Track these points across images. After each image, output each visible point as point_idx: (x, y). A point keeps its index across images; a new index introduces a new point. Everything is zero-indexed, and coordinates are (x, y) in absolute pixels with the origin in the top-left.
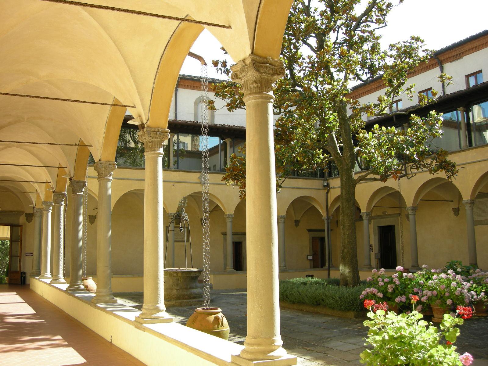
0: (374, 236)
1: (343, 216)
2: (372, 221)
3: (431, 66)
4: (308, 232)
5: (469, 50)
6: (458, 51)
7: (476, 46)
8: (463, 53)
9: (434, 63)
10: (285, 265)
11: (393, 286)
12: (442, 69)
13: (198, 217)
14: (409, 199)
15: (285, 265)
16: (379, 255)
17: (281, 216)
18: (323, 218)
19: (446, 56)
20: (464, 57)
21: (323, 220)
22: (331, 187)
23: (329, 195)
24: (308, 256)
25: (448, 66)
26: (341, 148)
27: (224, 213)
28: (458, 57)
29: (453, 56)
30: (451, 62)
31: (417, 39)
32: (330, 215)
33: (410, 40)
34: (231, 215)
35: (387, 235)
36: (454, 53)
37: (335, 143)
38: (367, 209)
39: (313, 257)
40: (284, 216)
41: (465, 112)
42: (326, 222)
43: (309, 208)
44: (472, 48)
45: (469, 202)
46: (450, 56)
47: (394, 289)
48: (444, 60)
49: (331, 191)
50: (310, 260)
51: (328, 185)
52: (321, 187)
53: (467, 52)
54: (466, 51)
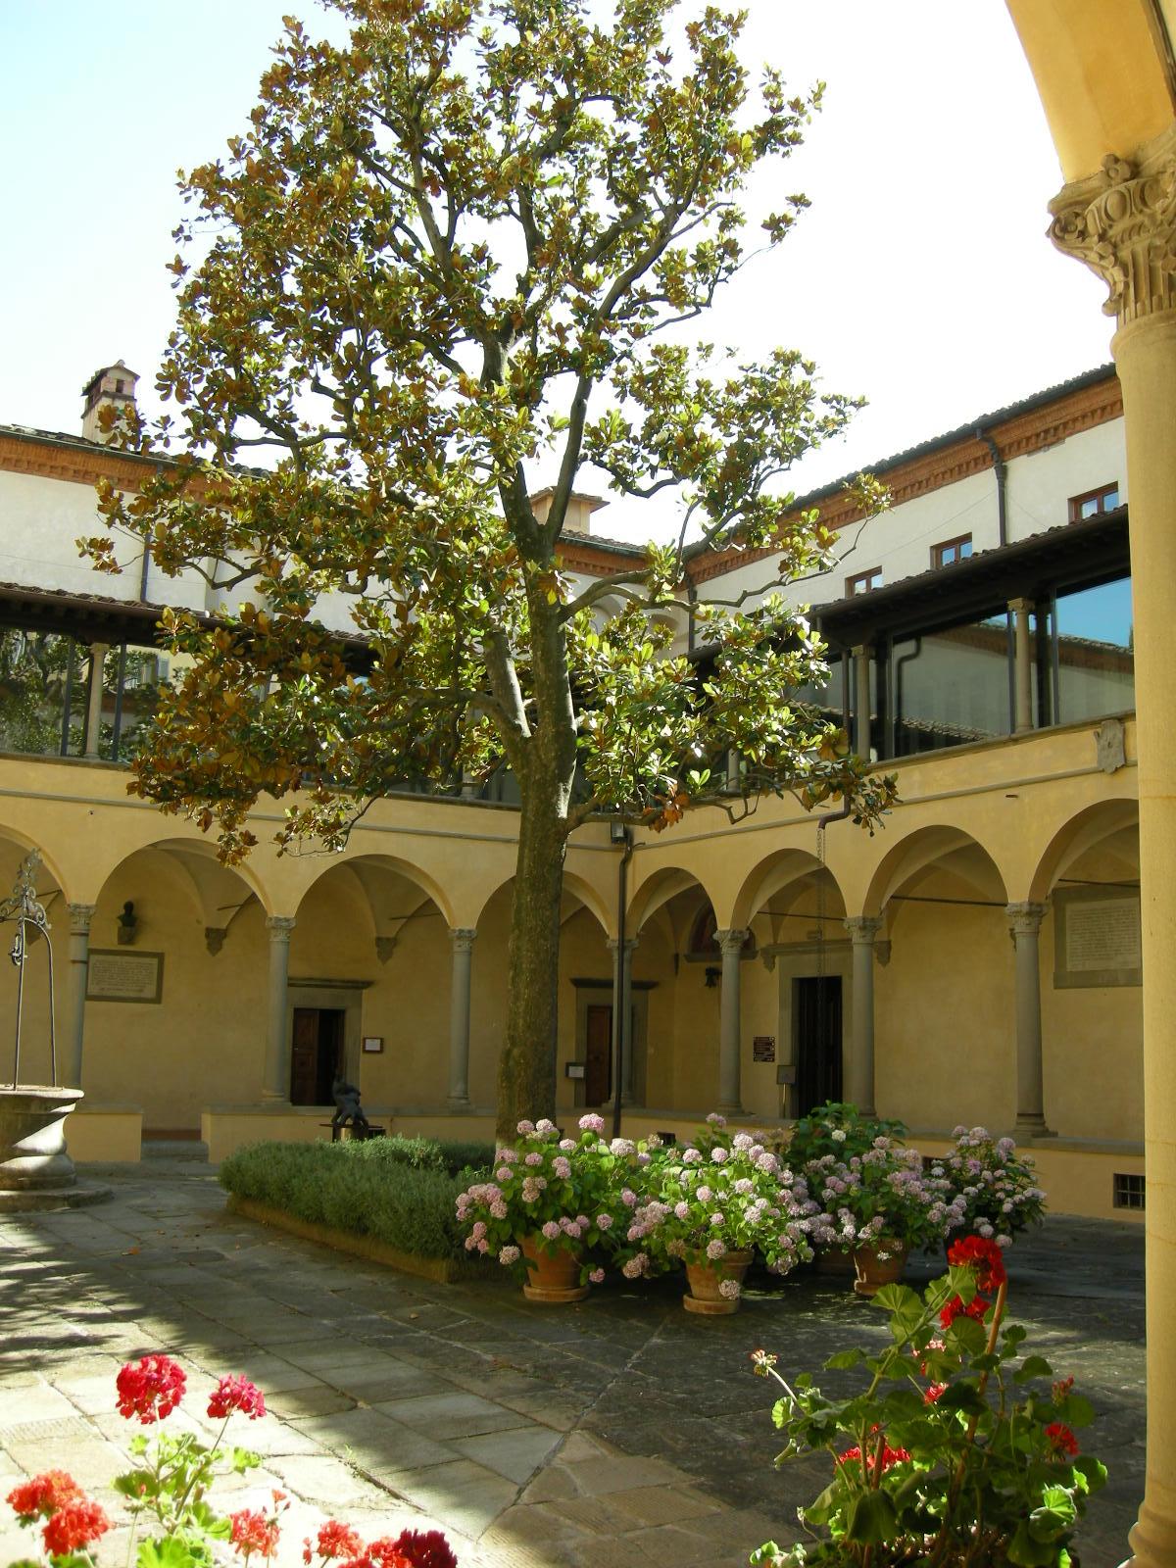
0: (782, 1007)
1: (519, 938)
2: (777, 960)
3: (972, 464)
4: (574, 988)
5: (1084, 417)
6: (1049, 419)
7: (1101, 404)
8: (1065, 425)
9: (979, 454)
10: (466, 1092)
11: (542, 1182)
12: (1002, 475)
13: (198, 922)
14: (855, 892)
15: (466, 1092)
16: (792, 1072)
17: (461, 931)
18: (609, 944)
19: (1015, 434)
20: (1067, 440)
21: (610, 950)
22: (636, 842)
23: (630, 869)
24: (568, 1065)
25: (1021, 467)
26: (531, 712)
27: (264, 913)
28: (1052, 437)
29: (1038, 435)
30: (1029, 453)
31: (789, 360)
32: (632, 934)
33: (769, 363)
34: (287, 920)
35: (819, 1005)
36: (1039, 426)
37: (513, 695)
38: (735, 920)
39: (587, 1072)
40: (470, 932)
41: (1031, 612)
42: (616, 956)
43: (575, 914)
44: (1093, 412)
45: (1025, 909)
46: (1028, 434)
47: (542, 1193)
48: (1011, 445)
49: (638, 855)
50: (577, 1080)
51: (628, 837)
52: (606, 843)
53: (1078, 425)
54: (1075, 420)
